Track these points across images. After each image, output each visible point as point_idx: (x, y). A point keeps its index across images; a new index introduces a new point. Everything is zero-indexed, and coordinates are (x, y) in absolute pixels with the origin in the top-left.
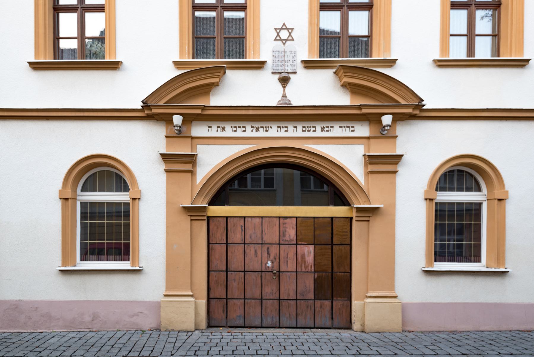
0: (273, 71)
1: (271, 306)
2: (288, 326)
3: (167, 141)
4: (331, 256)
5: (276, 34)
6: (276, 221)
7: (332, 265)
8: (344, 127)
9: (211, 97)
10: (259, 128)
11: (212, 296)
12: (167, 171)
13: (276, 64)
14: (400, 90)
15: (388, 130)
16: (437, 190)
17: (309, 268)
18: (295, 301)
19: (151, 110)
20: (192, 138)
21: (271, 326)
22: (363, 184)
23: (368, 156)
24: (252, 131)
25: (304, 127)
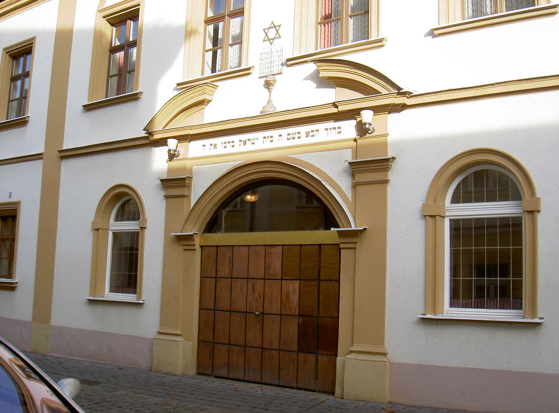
4: (317, 296)
7: (319, 307)
8: (330, 129)
17: (294, 309)
21: (253, 380)
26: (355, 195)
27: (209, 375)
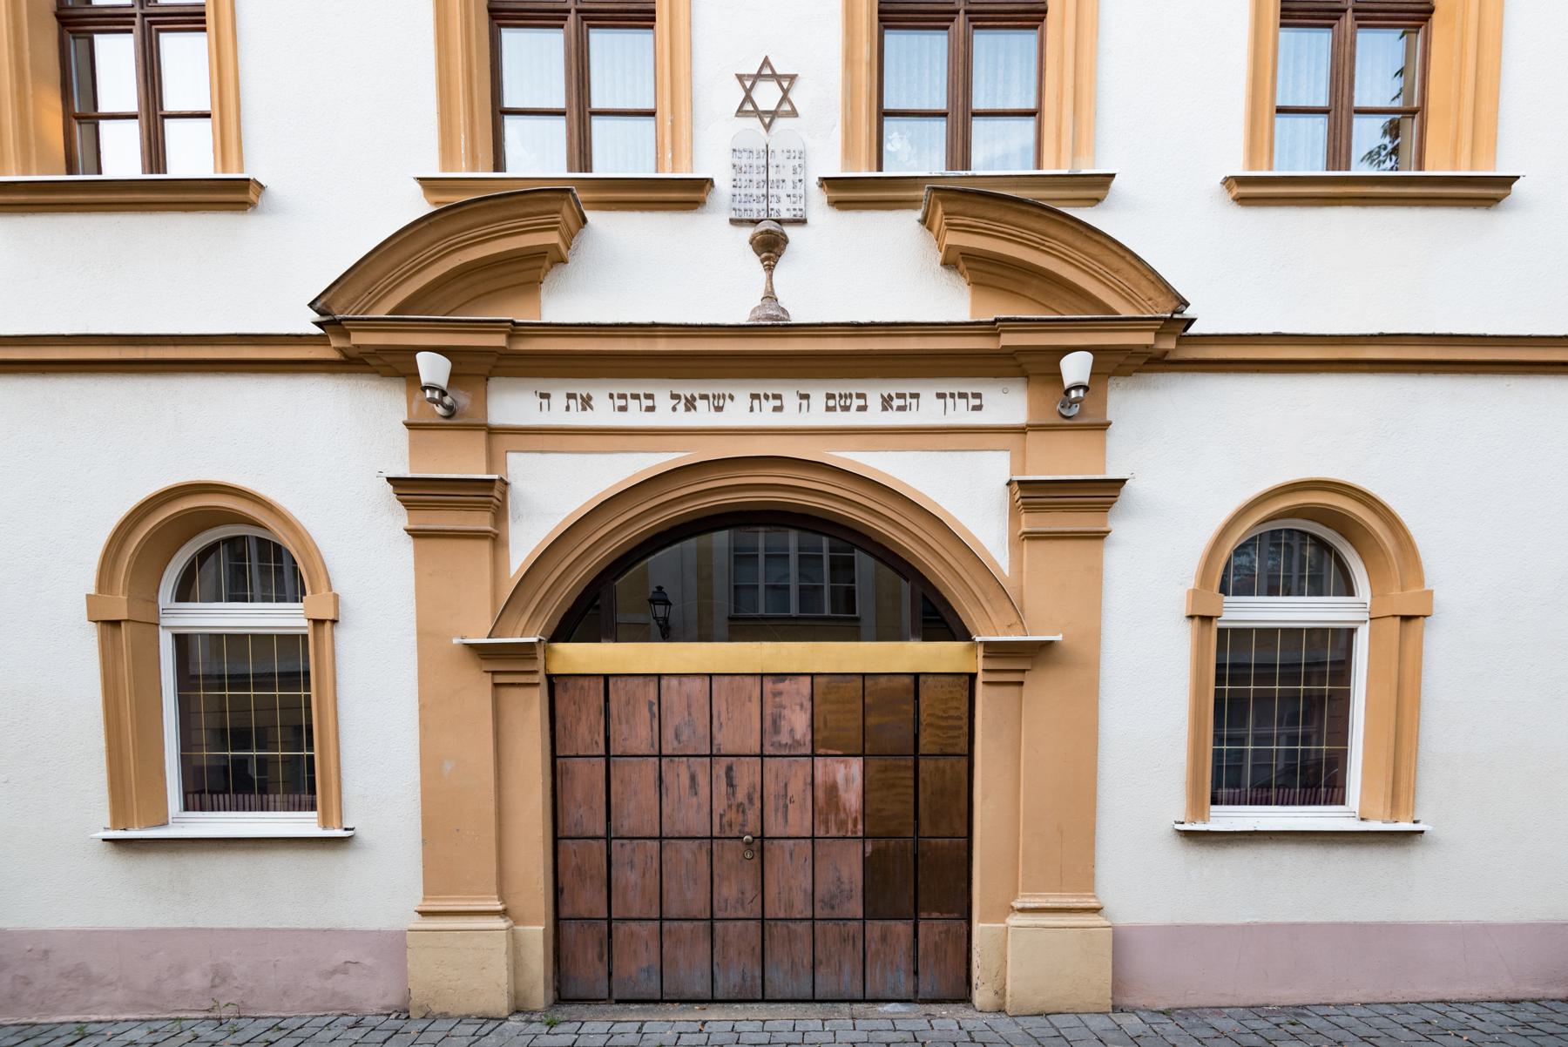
0: (733, 215)
1: (739, 937)
2: (789, 996)
3: (411, 441)
4: (912, 791)
5: (743, 95)
6: (753, 686)
8: (952, 395)
9: (543, 293)
10: (694, 398)
11: (565, 911)
12: (416, 534)
13: (743, 191)
14: (1117, 272)
15: (1078, 400)
16: (1224, 590)
18: (809, 923)
19: (347, 335)
20: (492, 431)
22: (1007, 572)
23: (1020, 482)
24: (674, 409)
25: (830, 396)
26: (1016, 560)
27: (597, 1001)
